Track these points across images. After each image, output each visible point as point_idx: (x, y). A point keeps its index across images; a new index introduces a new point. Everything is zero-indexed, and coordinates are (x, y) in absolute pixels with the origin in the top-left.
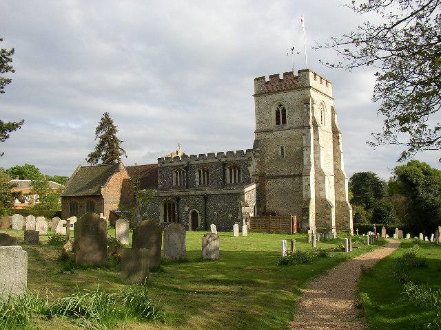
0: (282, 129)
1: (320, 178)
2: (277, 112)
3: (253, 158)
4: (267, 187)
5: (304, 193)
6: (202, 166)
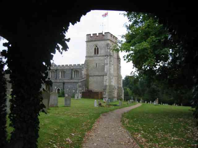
2: (95, 49)
4: (89, 79)
6: (63, 69)
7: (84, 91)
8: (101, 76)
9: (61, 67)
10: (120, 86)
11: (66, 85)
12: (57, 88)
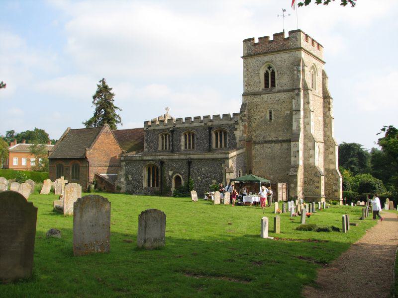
0: (271, 92)
1: (310, 145)
2: (266, 75)
3: (239, 121)
4: (254, 152)
5: (293, 159)
6: (187, 129)
8: (284, 141)
9: (221, 120)
10: (332, 167)
11: (194, 167)
12: (173, 175)
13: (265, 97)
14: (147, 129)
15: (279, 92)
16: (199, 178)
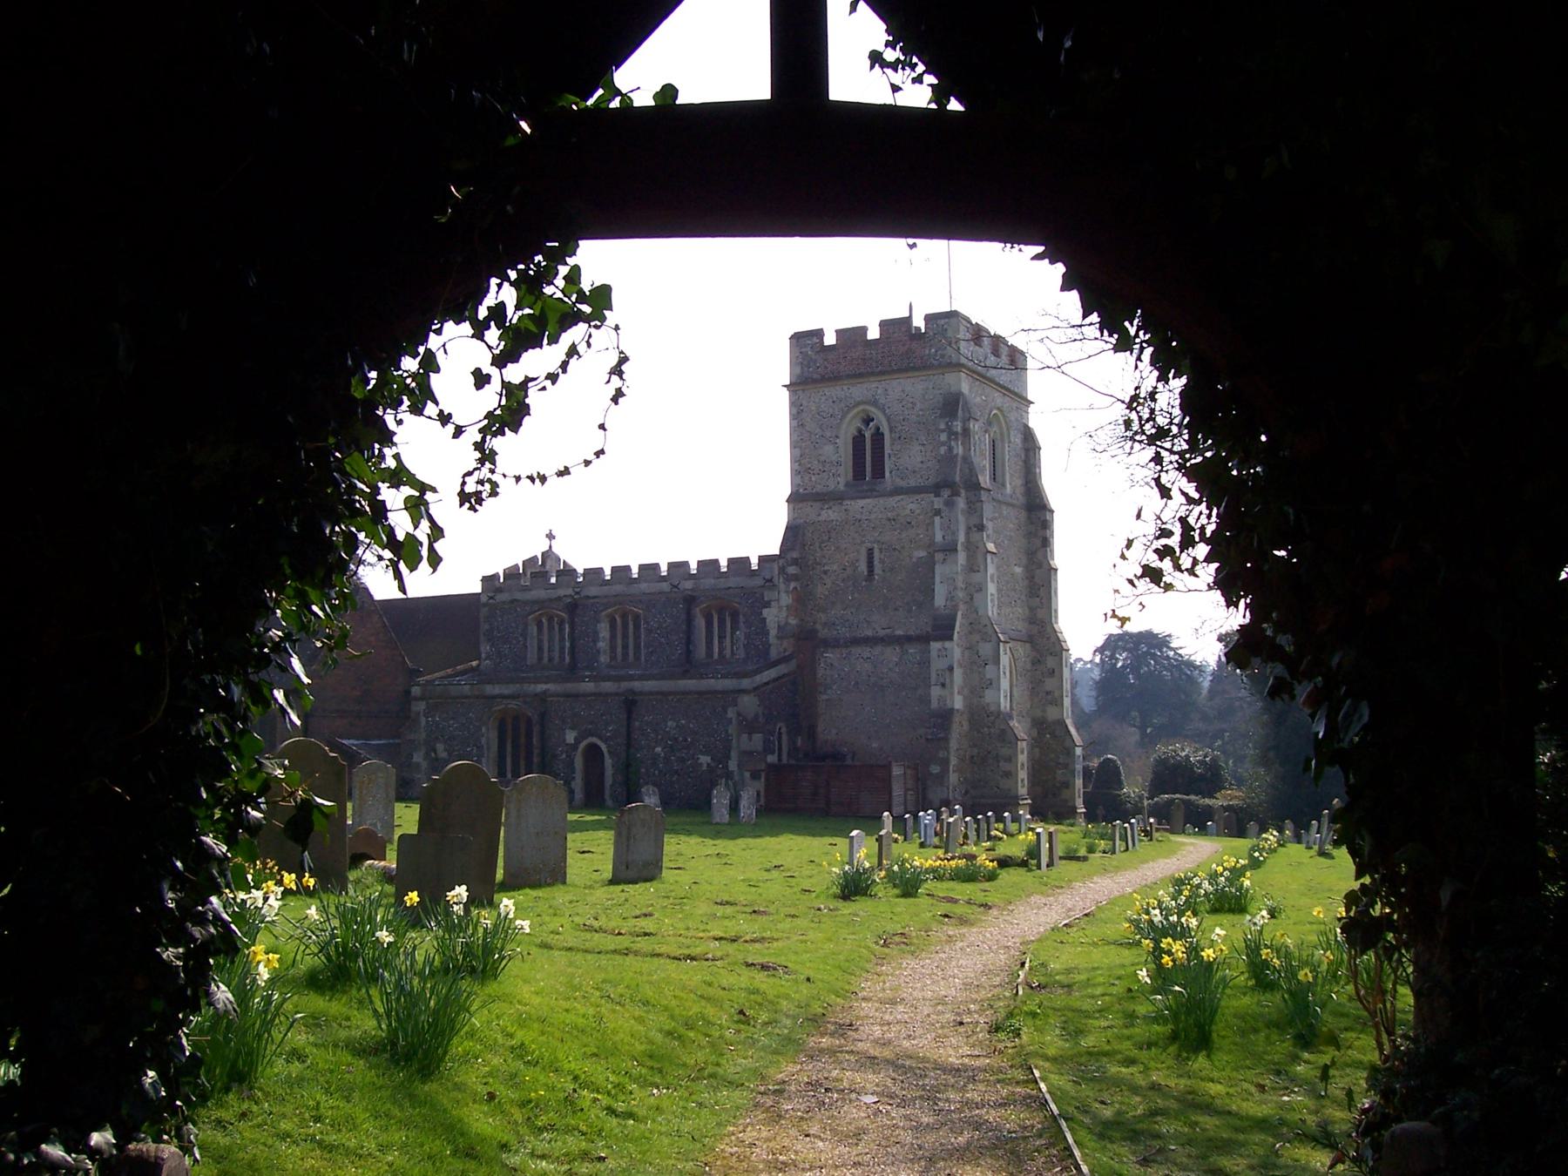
7: (785, 760)
10: (1052, 713)
12: (578, 741)
13: (857, 506)
14: (491, 598)
15: (897, 491)
16: (658, 749)
